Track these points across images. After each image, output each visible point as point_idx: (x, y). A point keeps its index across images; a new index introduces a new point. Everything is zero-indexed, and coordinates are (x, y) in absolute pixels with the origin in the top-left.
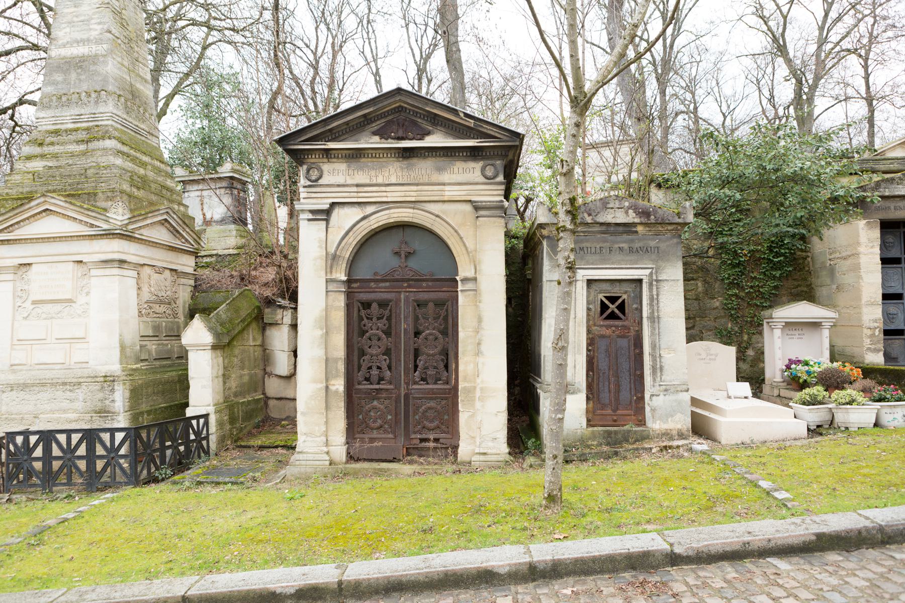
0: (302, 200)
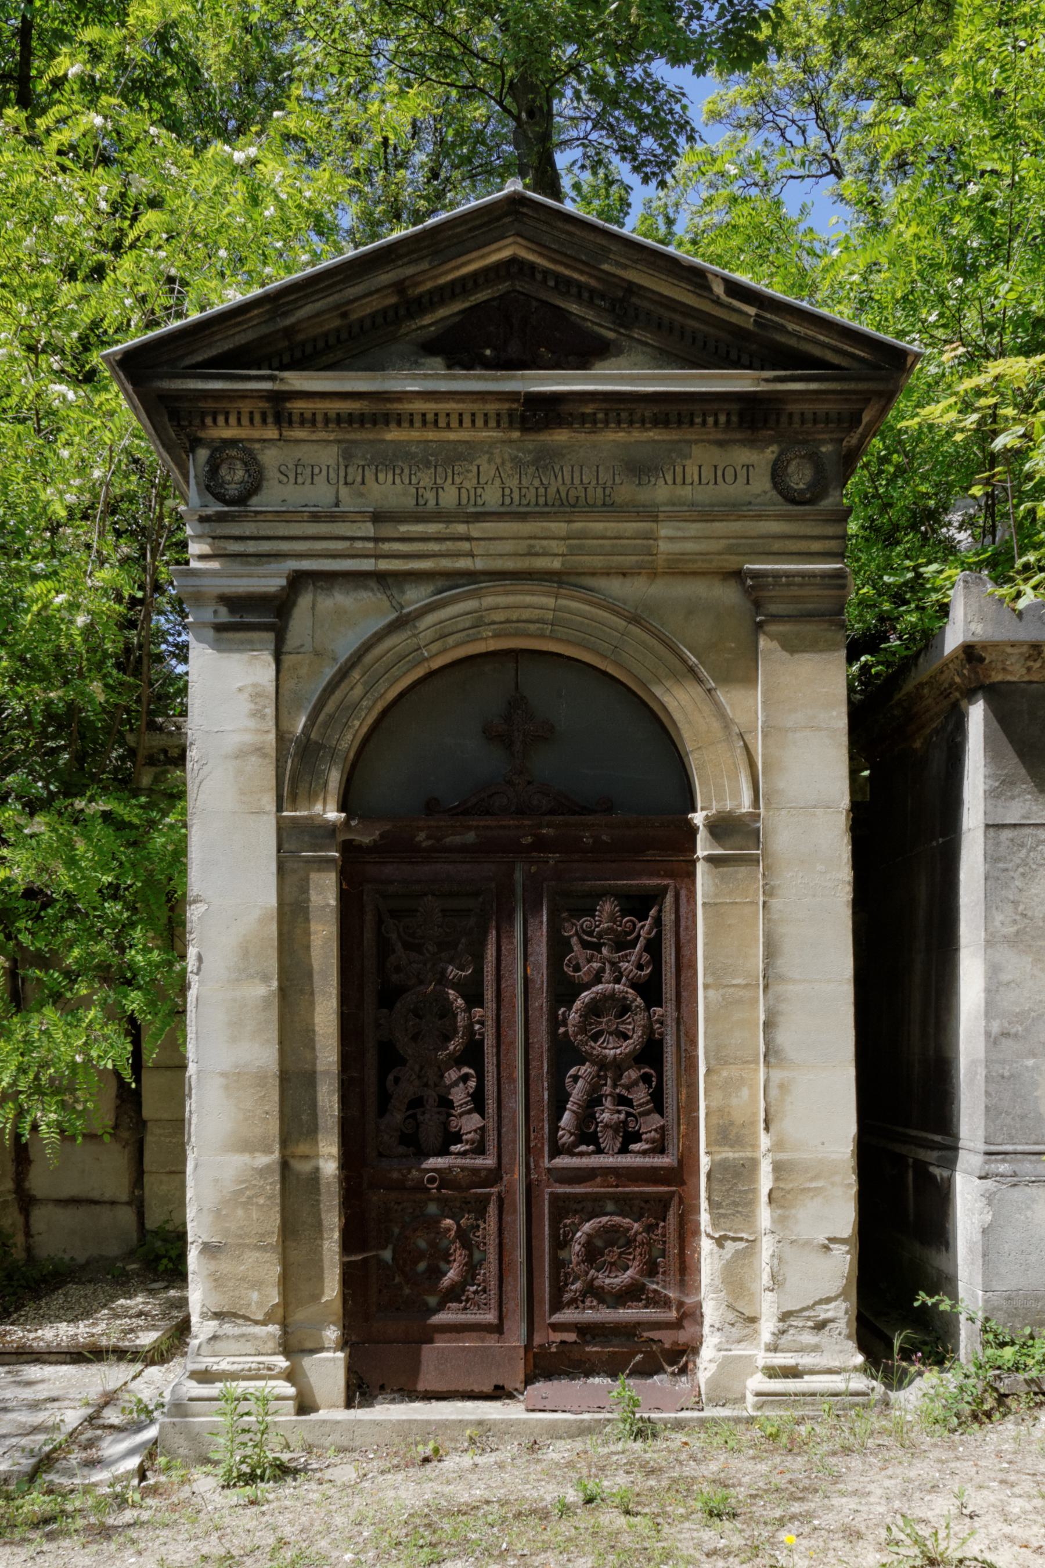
0: (194, 564)
